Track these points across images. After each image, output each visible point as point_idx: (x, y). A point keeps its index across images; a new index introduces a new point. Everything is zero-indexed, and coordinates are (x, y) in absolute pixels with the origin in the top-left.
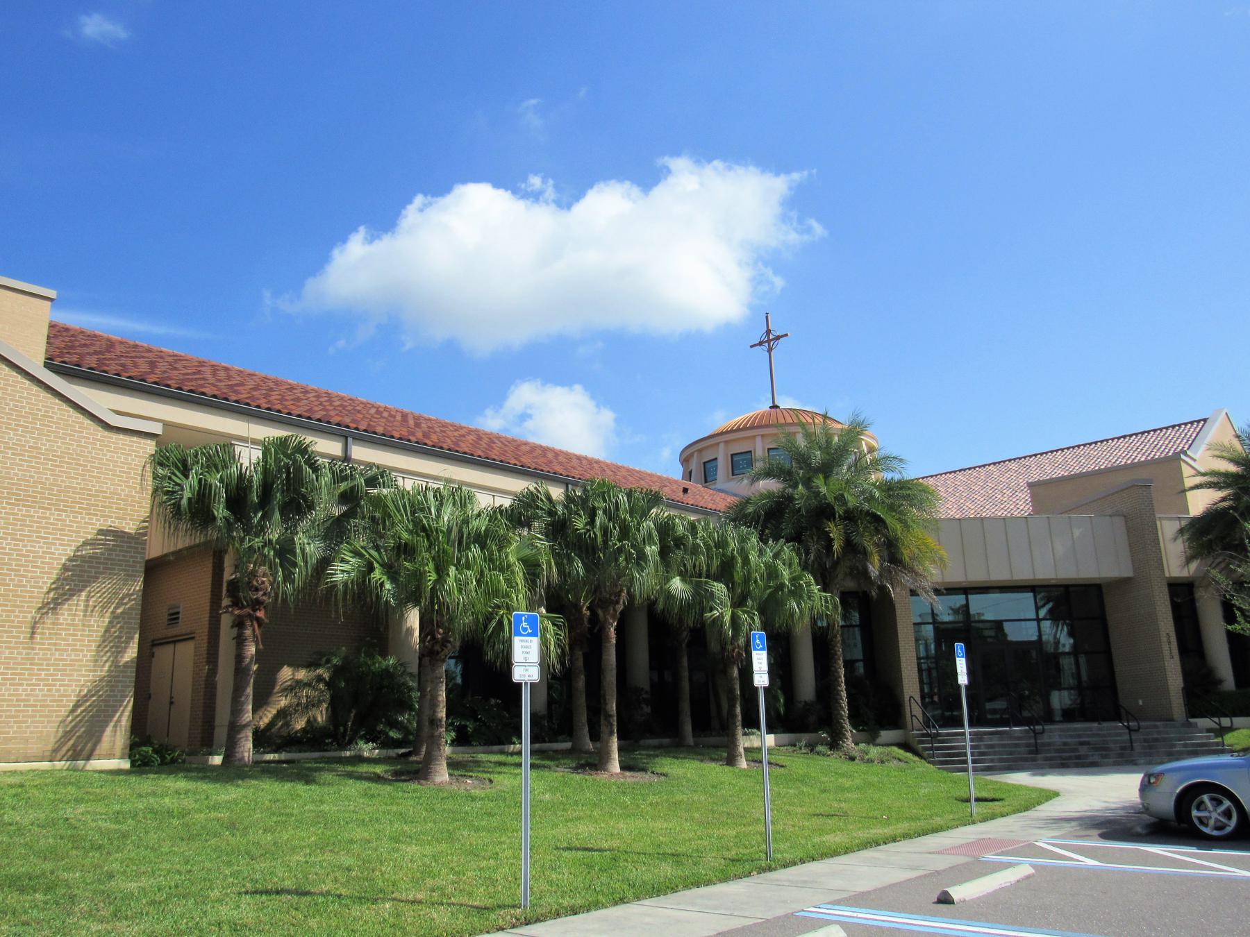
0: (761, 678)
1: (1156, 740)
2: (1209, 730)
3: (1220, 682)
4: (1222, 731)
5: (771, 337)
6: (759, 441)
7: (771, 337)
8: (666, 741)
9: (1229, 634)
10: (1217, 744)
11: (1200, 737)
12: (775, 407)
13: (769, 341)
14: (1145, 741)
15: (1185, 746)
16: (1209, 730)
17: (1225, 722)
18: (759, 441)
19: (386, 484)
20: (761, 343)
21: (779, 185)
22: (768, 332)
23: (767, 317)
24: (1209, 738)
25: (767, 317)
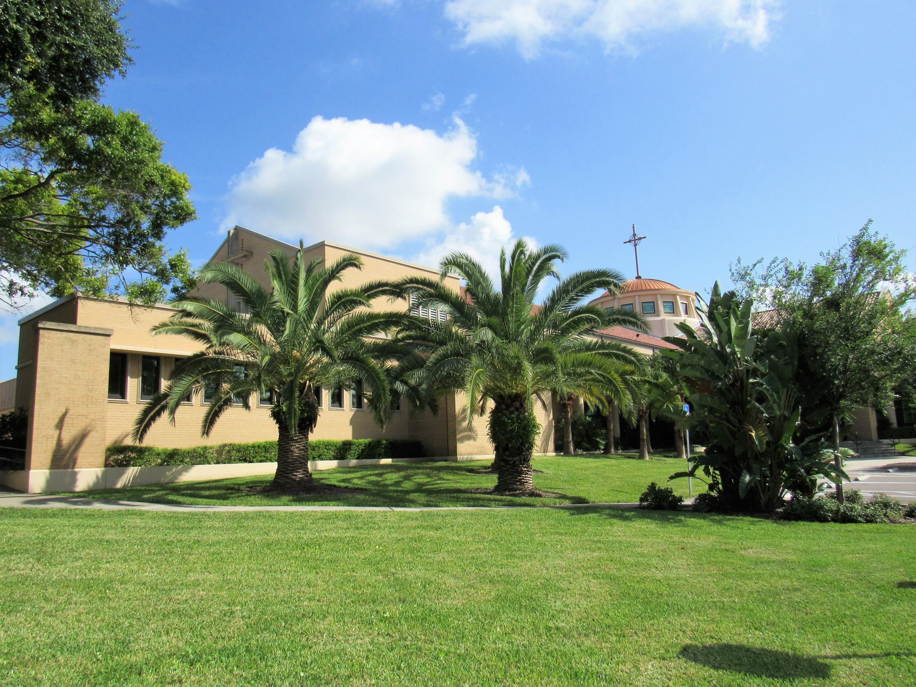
0: (411, 341)
1: (867, 448)
2: (888, 444)
3: (892, 424)
4: (894, 444)
5: (636, 238)
6: (637, 298)
7: (636, 238)
8: (662, 450)
9: (724, 320)
10: (892, 450)
11: (884, 447)
12: (638, 277)
13: (635, 240)
14: (862, 449)
15: (879, 450)
16: (888, 444)
17: (896, 441)
18: (637, 298)
19: (758, 421)
20: (630, 241)
21: (469, 39)
22: (634, 235)
23: (633, 227)
24: (888, 447)
25: (633, 227)
